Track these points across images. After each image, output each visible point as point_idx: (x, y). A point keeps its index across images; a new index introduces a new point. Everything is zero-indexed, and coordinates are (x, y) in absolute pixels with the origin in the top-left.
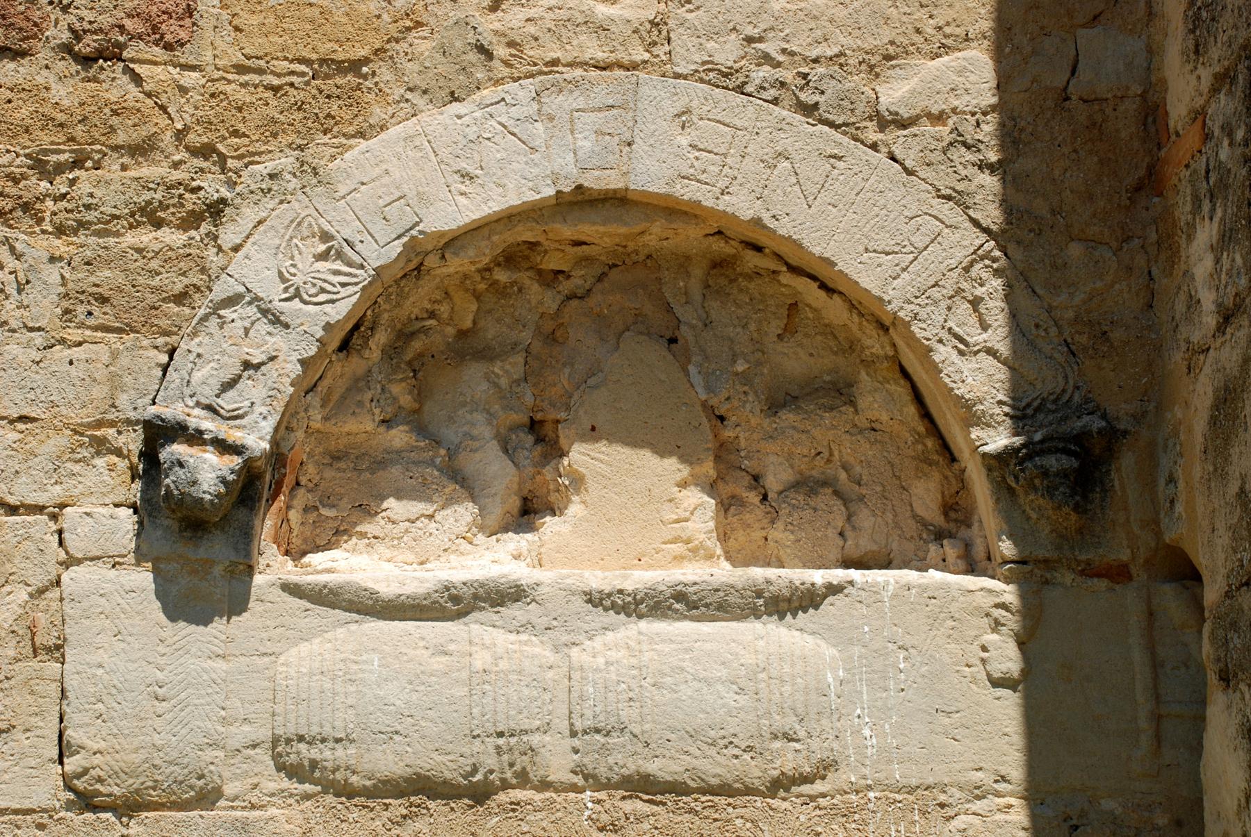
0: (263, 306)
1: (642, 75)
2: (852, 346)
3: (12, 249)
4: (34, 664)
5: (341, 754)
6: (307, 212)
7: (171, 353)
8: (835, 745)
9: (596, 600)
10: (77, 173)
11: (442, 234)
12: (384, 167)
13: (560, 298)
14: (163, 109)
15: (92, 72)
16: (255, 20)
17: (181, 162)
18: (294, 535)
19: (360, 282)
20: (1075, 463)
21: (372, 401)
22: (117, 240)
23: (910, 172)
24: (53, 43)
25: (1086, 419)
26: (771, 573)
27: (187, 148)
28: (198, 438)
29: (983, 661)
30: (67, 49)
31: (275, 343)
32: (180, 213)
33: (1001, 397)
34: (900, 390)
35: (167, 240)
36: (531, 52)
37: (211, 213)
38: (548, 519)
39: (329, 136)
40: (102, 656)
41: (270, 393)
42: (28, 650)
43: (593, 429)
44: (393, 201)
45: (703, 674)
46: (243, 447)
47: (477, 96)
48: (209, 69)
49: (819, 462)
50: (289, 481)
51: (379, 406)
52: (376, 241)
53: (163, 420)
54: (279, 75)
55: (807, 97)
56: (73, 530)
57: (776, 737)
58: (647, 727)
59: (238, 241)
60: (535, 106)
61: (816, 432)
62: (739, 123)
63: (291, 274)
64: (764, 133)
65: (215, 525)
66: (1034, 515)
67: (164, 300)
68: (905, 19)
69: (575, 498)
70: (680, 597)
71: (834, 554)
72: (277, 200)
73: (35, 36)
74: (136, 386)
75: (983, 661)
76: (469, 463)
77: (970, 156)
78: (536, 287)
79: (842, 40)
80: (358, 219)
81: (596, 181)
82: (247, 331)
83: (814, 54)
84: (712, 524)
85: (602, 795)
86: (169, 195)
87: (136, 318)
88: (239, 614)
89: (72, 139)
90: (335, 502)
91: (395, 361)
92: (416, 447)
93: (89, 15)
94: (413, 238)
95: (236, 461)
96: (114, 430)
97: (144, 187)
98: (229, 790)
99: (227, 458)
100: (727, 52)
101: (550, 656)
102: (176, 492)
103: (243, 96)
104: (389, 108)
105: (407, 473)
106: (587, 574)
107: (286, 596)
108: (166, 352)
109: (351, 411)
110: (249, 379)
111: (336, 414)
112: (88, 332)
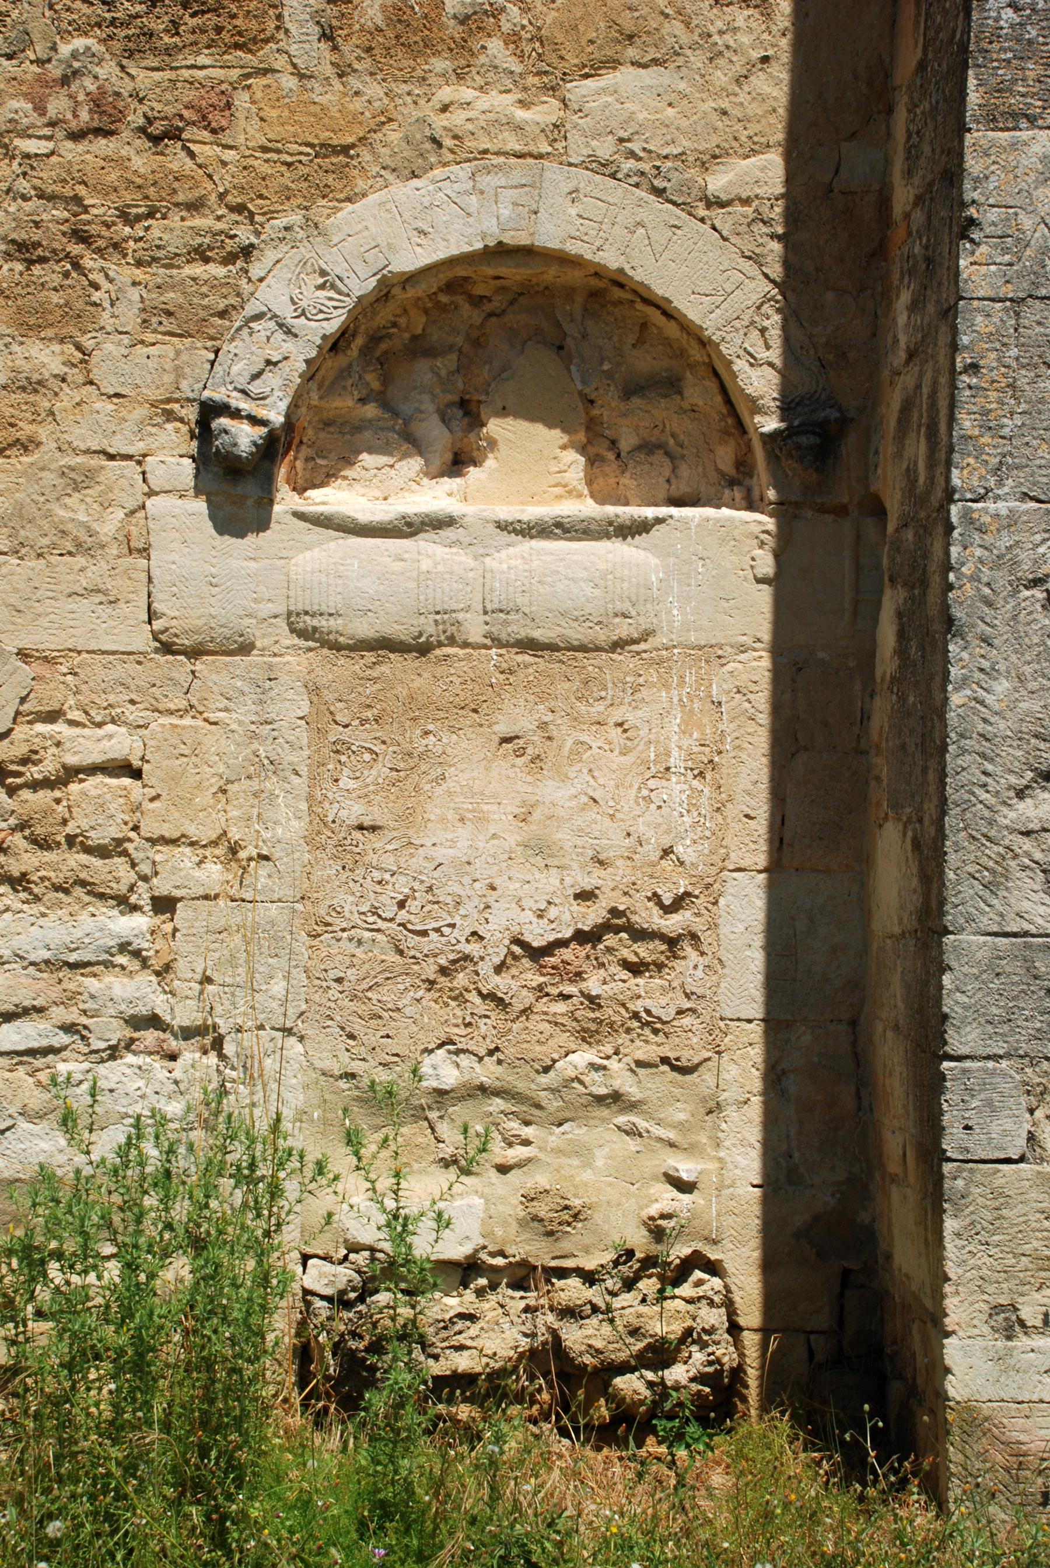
1: (546, 163)
2: (681, 353)
3: (107, 276)
4: (130, 559)
5: (333, 623)
7: (217, 352)
8: (655, 621)
9: (502, 526)
10: (150, 222)
11: (403, 273)
13: (483, 315)
14: (210, 176)
15: (160, 148)
16: (274, 113)
17: (223, 216)
20: (818, 440)
23: (725, 239)
24: (133, 126)
25: (828, 411)
26: (620, 510)
27: (227, 206)
29: (752, 567)
30: (142, 130)
33: (775, 395)
34: (712, 385)
35: (213, 272)
36: (469, 143)
38: (471, 469)
40: (175, 557)
42: (126, 551)
43: (504, 408)
45: (571, 575)
47: (431, 174)
48: (242, 148)
49: (656, 432)
50: (296, 441)
54: (291, 155)
55: (658, 183)
56: (153, 473)
57: (616, 615)
58: (534, 609)
60: (471, 183)
61: (655, 412)
62: (611, 201)
64: (628, 208)
65: (248, 472)
66: (790, 473)
67: (211, 315)
68: (727, 130)
69: (490, 455)
70: (558, 525)
71: (662, 495)
73: (120, 120)
75: (752, 567)
76: (419, 429)
77: (765, 230)
78: (467, 306)
79: (685, 143)
81: (510, 239)
82: (268, 338)
83: (664, 152)
84: (582, 475)
85: (503, 651)
87: (192, 327)
88: (264, 531)
89: (147, 197)
93: (158, 106)
94: (384, 276)
95: (265, 430)
98: (258, 644)
99: (257, 428)
100: (605, 149)
101: (471, 563)
103: (265, 169)
106: (497, 509)
107: (295, 520)
112: (159, 336)
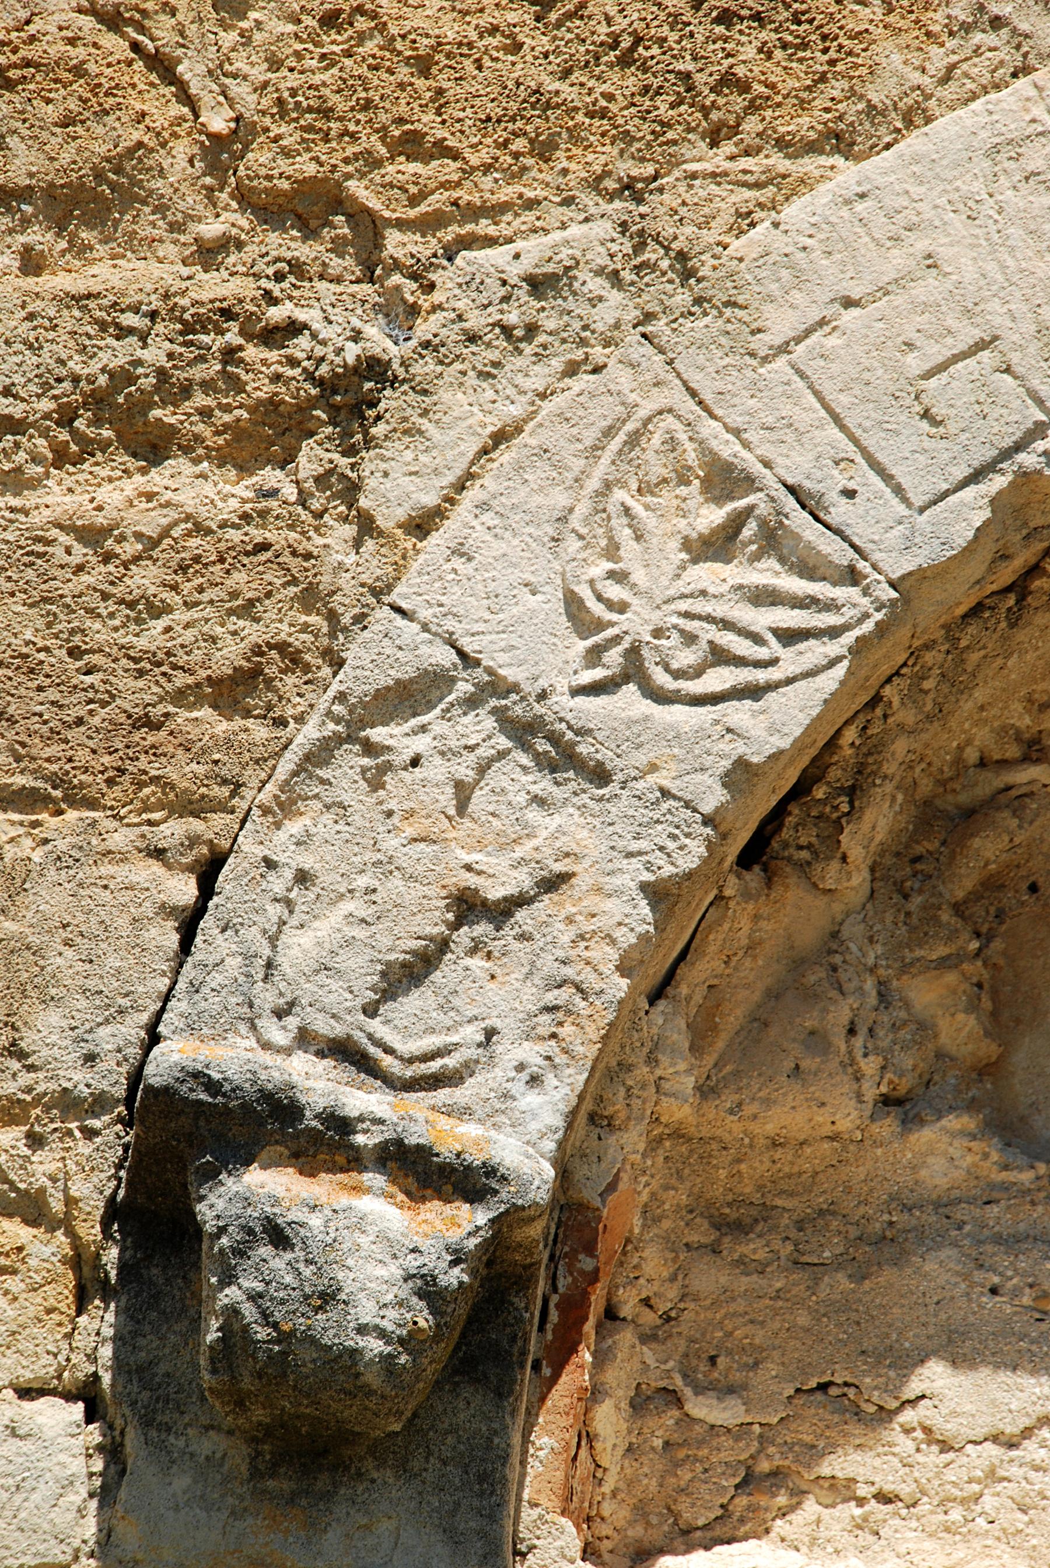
0: (518, 710)
6: (658, 400)
12: (922, 245)
17: (227, 244)
18: (607, 1488)
19: (846, 628)
21: (852, 1031)
22: (15, 502)
27: (244, 197)
28: (335, 1147)
31: (560, 830)
32: (227, 409)
37: (334, 410)
39: (728, 148)
41: (551, 997)
44: (956, 359)
46: (490, 1171)
51: (877, 1051)
52: (899, 490)
53: (212, 1087)
59: (430, 499)
63: (610, 605)
67: (179, 697)
72: (557, 364)
74: (92, 984)
80: (837, 419)
82: (463, 792)
86: (190, 354)
90: (737, 1377)
91: (917, 900)
92: (1006, 1187)
94: (1024, 476)
96: (18, 1132)
97: (103, 326)
99: (434, 1211)
102: (262, 1333)
104: (934, 50)
105: (978, 1276)
108: (190, 869)
109: (789, 1065)
110: (473, 951)
111: (737, 1074)
